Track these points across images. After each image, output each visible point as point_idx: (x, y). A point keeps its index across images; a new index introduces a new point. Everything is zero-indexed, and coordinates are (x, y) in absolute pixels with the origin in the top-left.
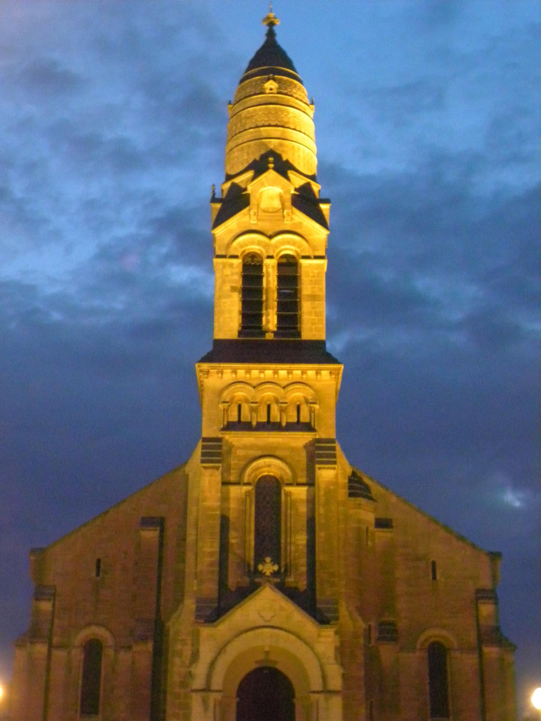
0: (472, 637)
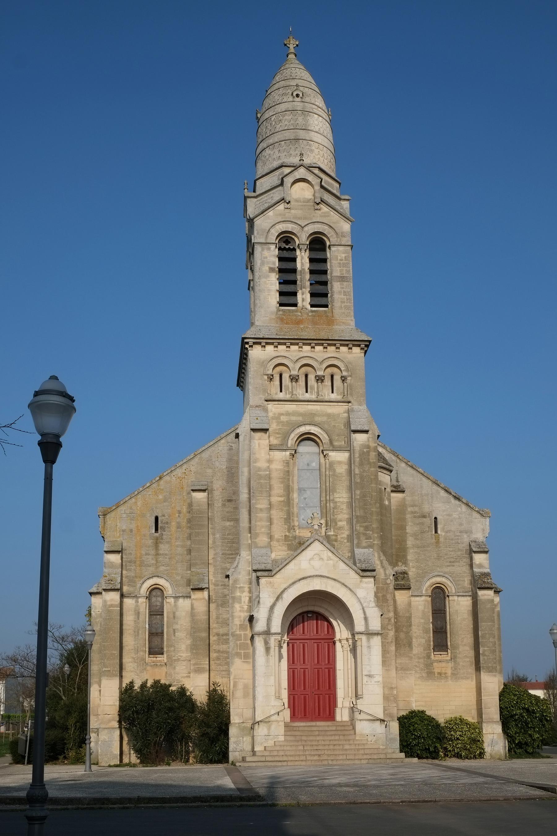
0: (466, 583)
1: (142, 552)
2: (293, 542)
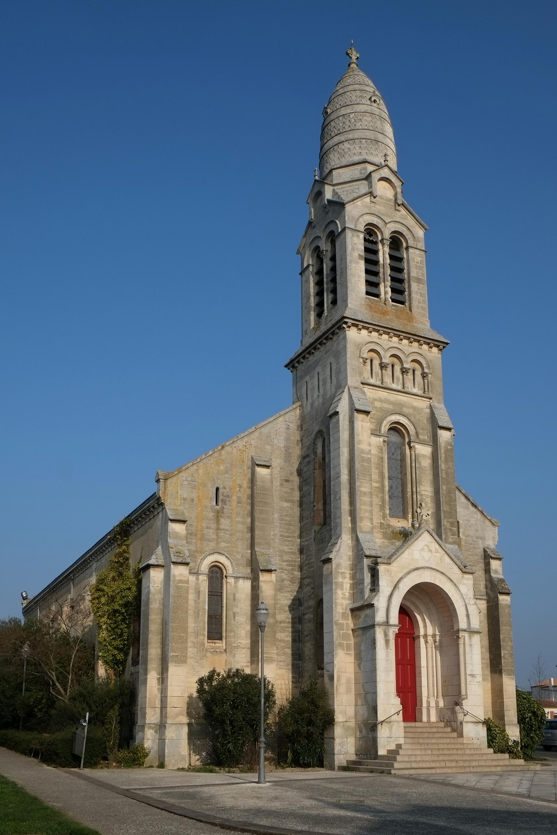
1: (203, 525)
2: (388, 531)
